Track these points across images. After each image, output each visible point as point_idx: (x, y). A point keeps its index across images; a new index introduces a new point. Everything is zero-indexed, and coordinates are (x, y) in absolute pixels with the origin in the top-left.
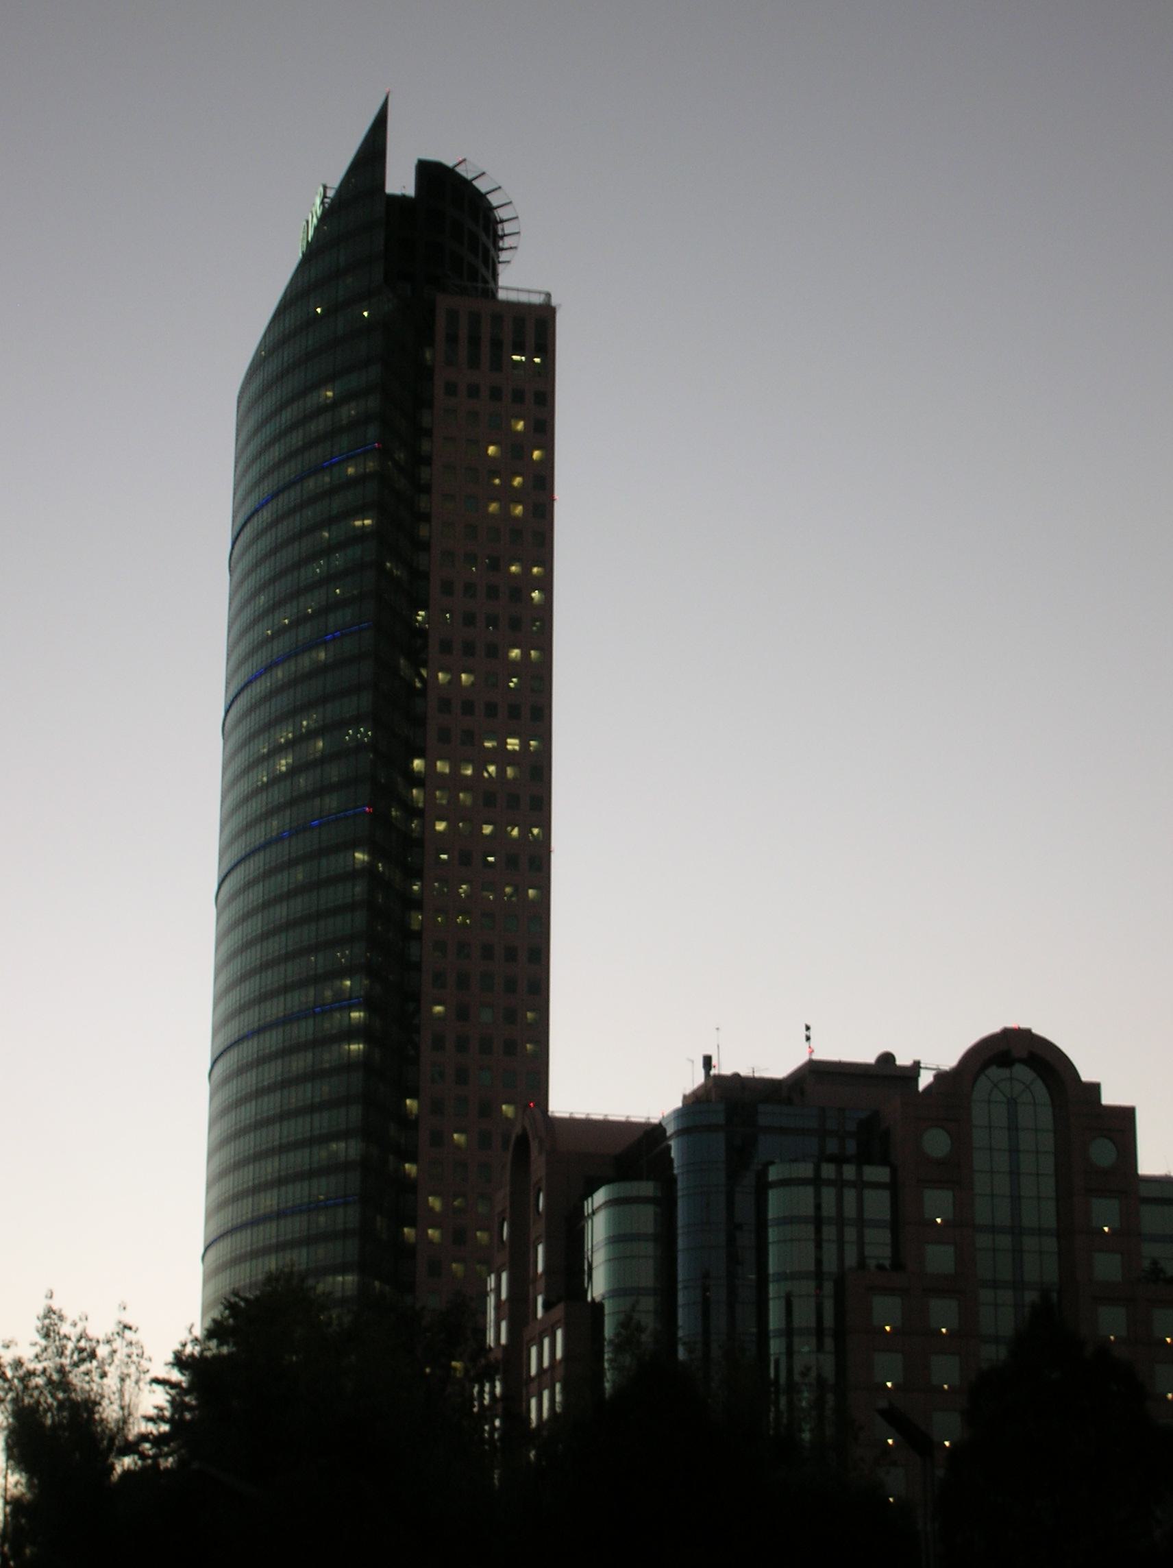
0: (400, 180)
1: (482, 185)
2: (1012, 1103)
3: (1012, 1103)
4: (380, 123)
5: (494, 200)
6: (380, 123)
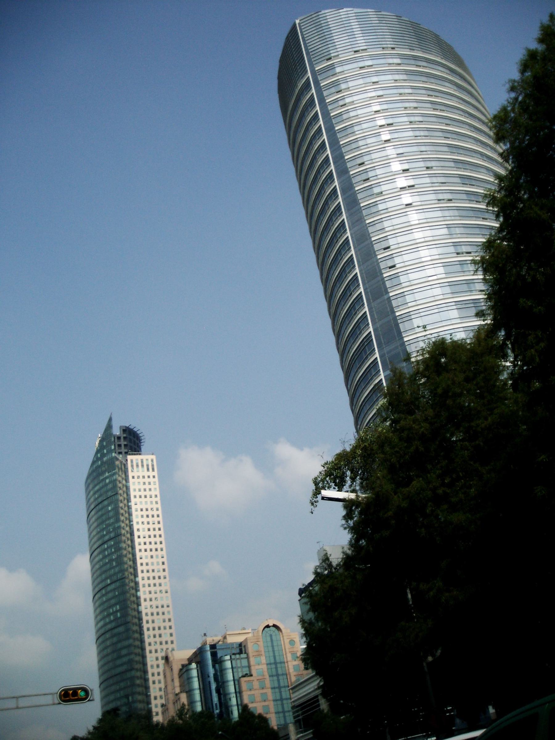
0: (116, 431)
1: (135, 430)
2: (271, 636)
3: (271, 636)
4: (110, 420)
5: (138, 432)
6: (110, 420)
